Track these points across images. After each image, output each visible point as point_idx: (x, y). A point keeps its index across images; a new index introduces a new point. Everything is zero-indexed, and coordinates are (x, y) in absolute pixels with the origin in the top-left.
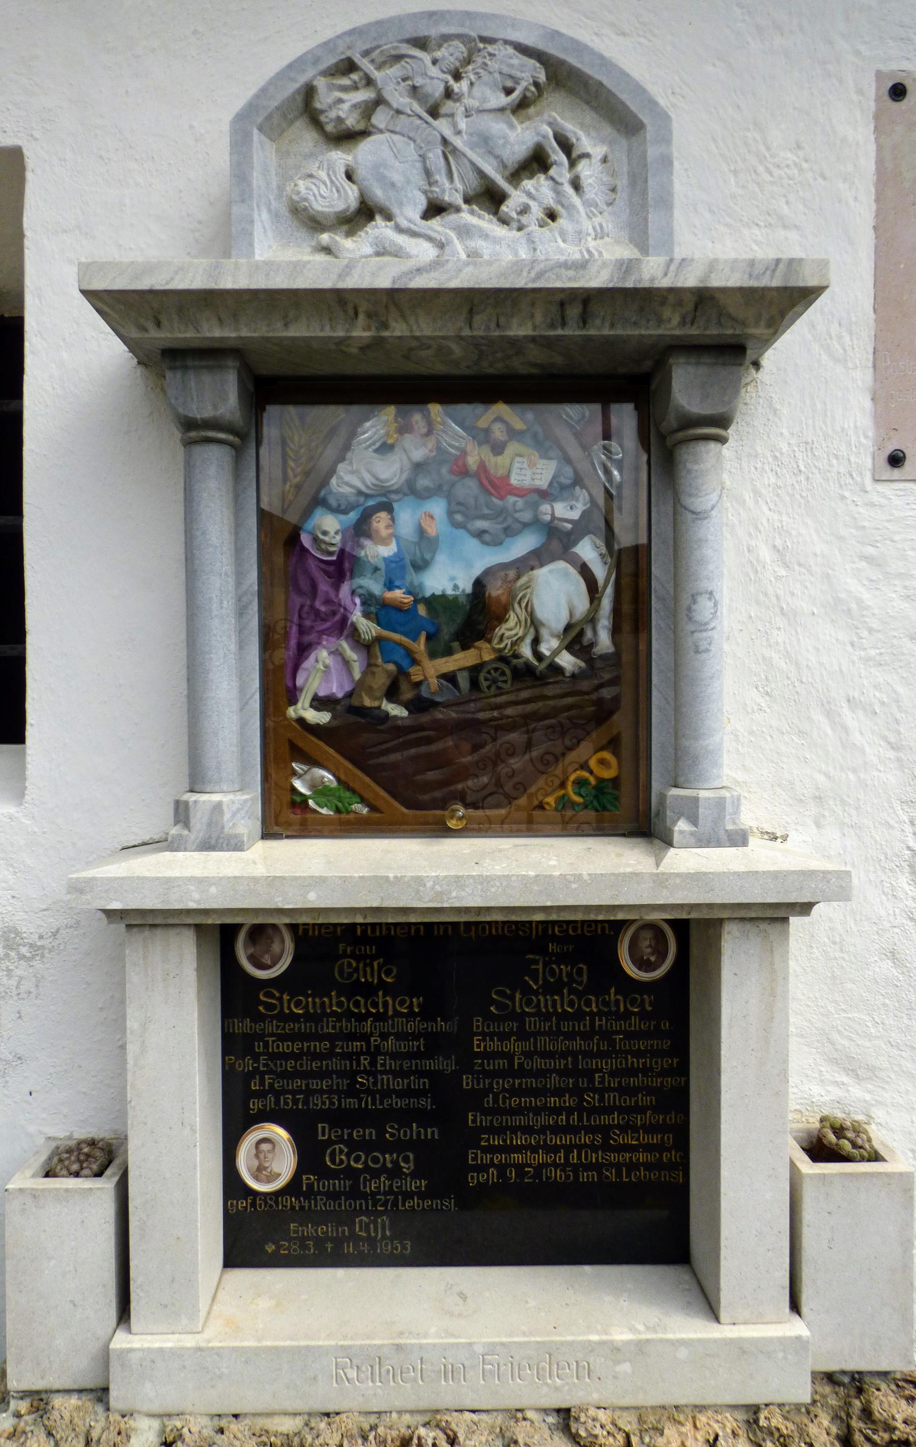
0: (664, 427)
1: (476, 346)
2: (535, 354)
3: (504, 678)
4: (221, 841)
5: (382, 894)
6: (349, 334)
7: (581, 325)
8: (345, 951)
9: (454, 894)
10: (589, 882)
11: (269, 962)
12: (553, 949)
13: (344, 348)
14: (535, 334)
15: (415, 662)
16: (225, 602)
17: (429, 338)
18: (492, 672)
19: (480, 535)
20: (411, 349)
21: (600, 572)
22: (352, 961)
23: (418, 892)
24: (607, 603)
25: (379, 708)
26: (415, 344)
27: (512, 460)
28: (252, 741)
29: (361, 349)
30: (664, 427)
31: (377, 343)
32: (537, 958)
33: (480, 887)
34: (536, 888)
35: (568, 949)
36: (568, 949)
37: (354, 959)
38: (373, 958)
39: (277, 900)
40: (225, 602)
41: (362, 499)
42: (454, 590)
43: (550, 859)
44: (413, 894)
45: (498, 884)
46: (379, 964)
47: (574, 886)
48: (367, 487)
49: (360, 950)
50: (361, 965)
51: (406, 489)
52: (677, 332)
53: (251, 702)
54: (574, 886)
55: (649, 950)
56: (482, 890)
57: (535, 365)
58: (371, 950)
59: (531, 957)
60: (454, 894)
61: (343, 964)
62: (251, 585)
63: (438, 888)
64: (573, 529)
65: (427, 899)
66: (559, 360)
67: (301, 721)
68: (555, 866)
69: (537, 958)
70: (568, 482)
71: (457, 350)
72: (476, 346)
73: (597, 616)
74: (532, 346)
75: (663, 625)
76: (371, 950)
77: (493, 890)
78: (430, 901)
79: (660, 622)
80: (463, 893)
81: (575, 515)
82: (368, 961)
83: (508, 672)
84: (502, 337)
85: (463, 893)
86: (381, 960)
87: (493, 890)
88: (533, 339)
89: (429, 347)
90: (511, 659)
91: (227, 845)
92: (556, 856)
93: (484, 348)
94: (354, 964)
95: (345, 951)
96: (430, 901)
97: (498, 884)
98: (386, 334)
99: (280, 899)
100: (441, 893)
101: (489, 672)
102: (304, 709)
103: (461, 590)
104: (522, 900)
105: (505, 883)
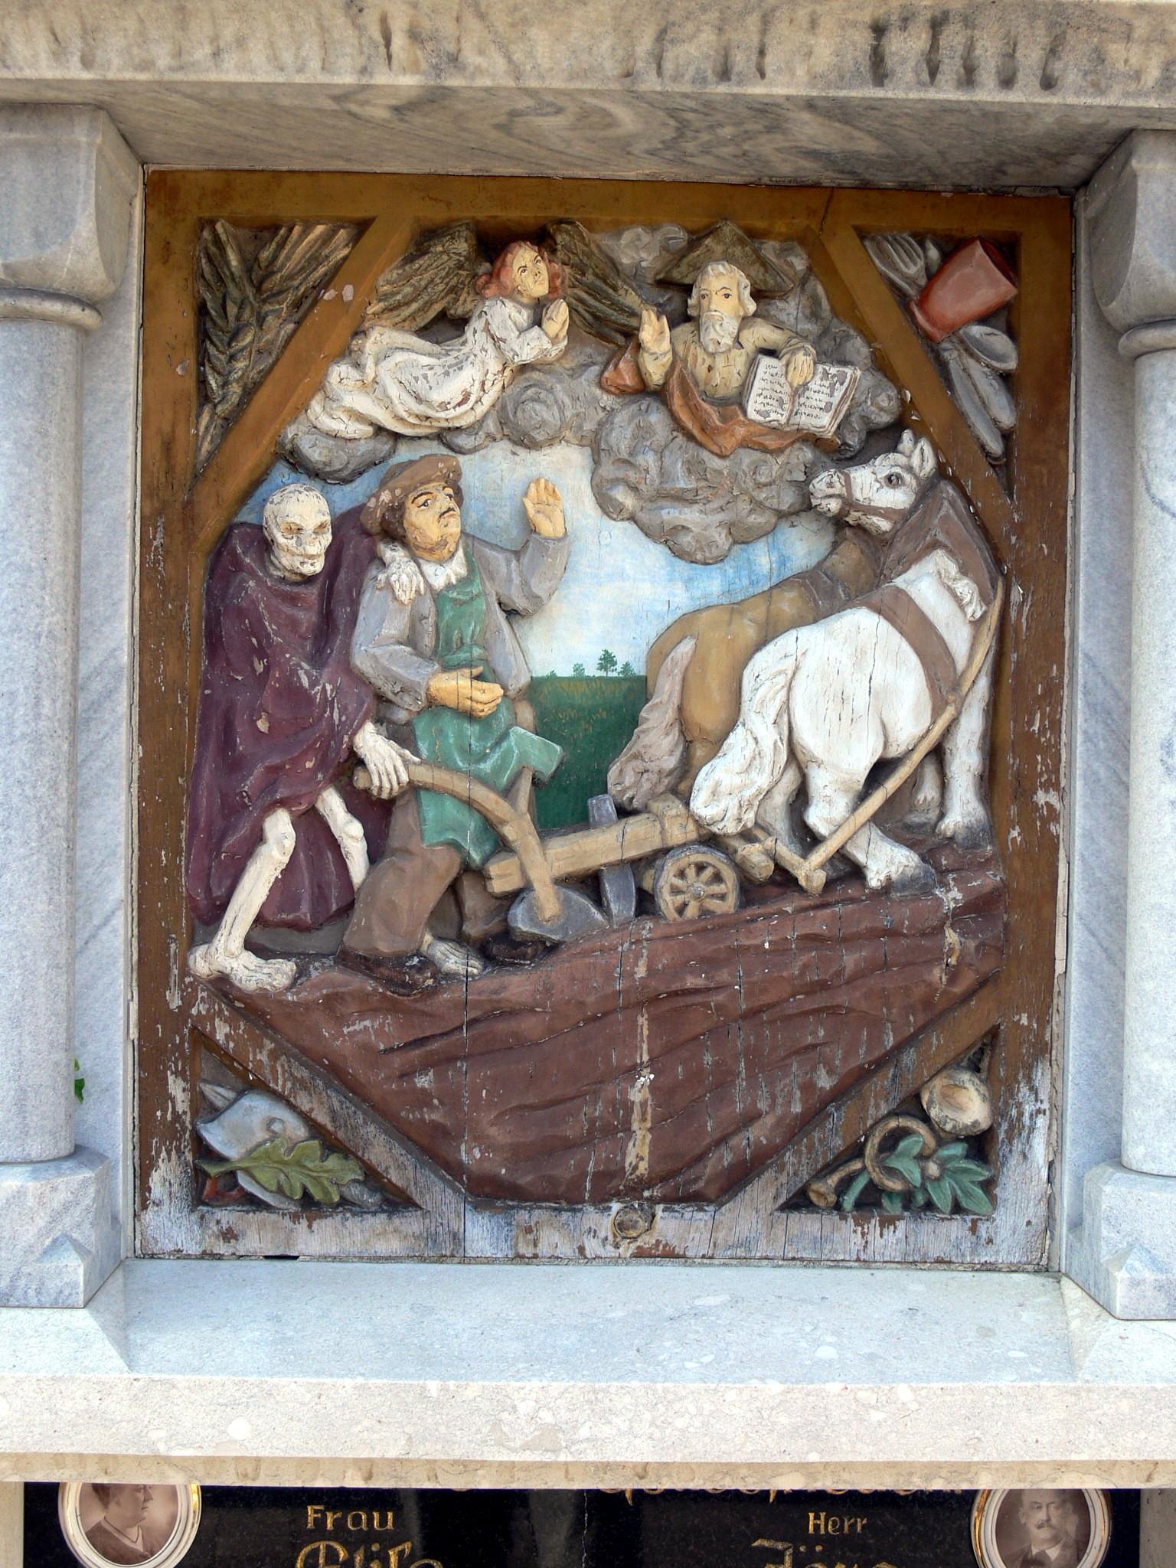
0: (1115, 309)
1: (672, 113)
2: (810, 131)
3: (717, 889)
4: (22, 1282)
5: (409, 1429)
6: (364, 81)
7: (925, 76)
8: (320, 1523)
9: (584, 1432)
10: (914, 1406)
11: (139, 1547)
12: (817, 1527)
13: (354, 108)
14: (814, 93)
15: (502, 846)
16: (46, 702)
17: (558, 92)
18: (691, 872)
19: (668, 537)
20: (514, 114)
21: (958, 638)
22: (338, 1547)
23: (497, 1424)
24: (971, 726)
25: (423, 1120)
26: (528, 102)
27: (752, 364)
28: (105, 1028)
29: (397, 109)
30: (1115, 309)
31: (433, 99)
32: (780, 1546)
33: (647, 1416)
34: (783, 1420)
35: (853, 1526)
36: (853, 1526)
37: (345, 1544)
38: (390, 1540)
39: (154, 1435)
40: (46, 702)
41: (384, 446)
42: (602, 667)
43: (817, 1343)
44: (485, 1430)
45: (692, 1410)
46: (401, 1554)
47: (876, 1416)
48: (401, 420)
49: (357, 1521)
50: (359, 1558)
51: (491, 425)
52: (1152, 103)
53: (104, 935)
54: (876, 1416)
55: (1044, 1534)
56: (652, 1423)
57: (813, 154)
58: (383, 1522)
59: (766, 1543)
60: (584, 1432)
61: (315, 1553)
62: (113, 653)
63: (547, 1417)
64: (895, 532)
65: (518, 1443)
66: (868, 145)
67: (221, 984)
68: (830, 1363)
69: (780, 1546)
70: (885, 419)
71: (627, 119)
72: (672, 113)
73: (948, 746)
74: (806, 116)
75: (1102, 773)
76: (383, 1522)
77: (680, 1423)
78: (526, 1447)
79: (1096, 765)
80: (607, 1431)
81: (899, 499)
82: (375, 1548)
83: (729, 875)
84: (736, 97)
85: (607, 1431)
86: (407, 1547)
87: (680, 1423)
88: (810, 105)
89: (559, 111)
90: (736, 843)
91: (38, 1292)
92: (834, 1333)
93: (690, 116)
94: (342, 1554)
95: (320, 1523)
96: (526, 1447)
97: (692, 1410)
98: (454, 81)
99: (162, 1434)
100: (556, 1428)
101: (682, 874)
102: (233, 955)
103: (619, 667)
104: (749, 1447)
105: (708, 1408)
